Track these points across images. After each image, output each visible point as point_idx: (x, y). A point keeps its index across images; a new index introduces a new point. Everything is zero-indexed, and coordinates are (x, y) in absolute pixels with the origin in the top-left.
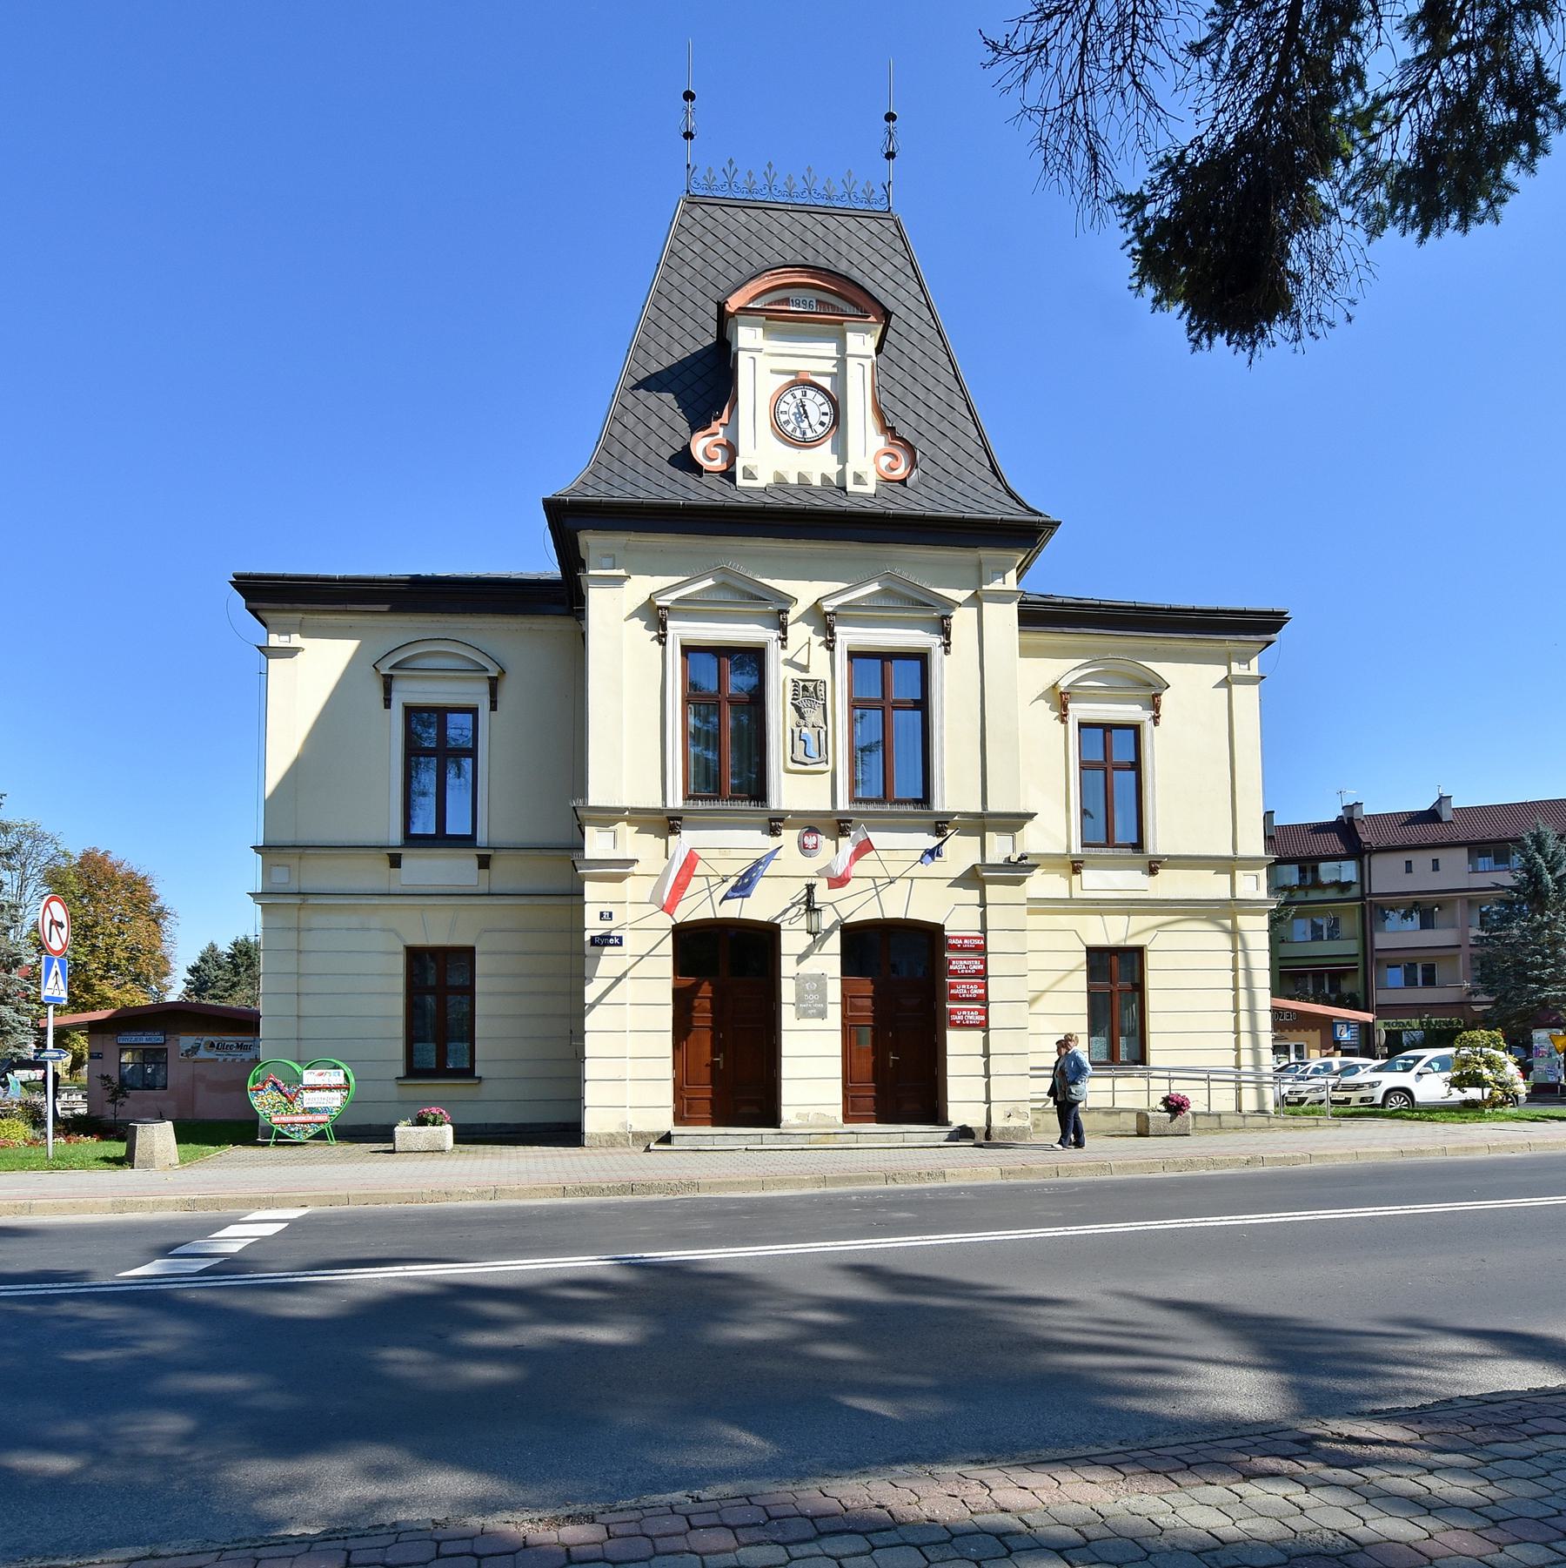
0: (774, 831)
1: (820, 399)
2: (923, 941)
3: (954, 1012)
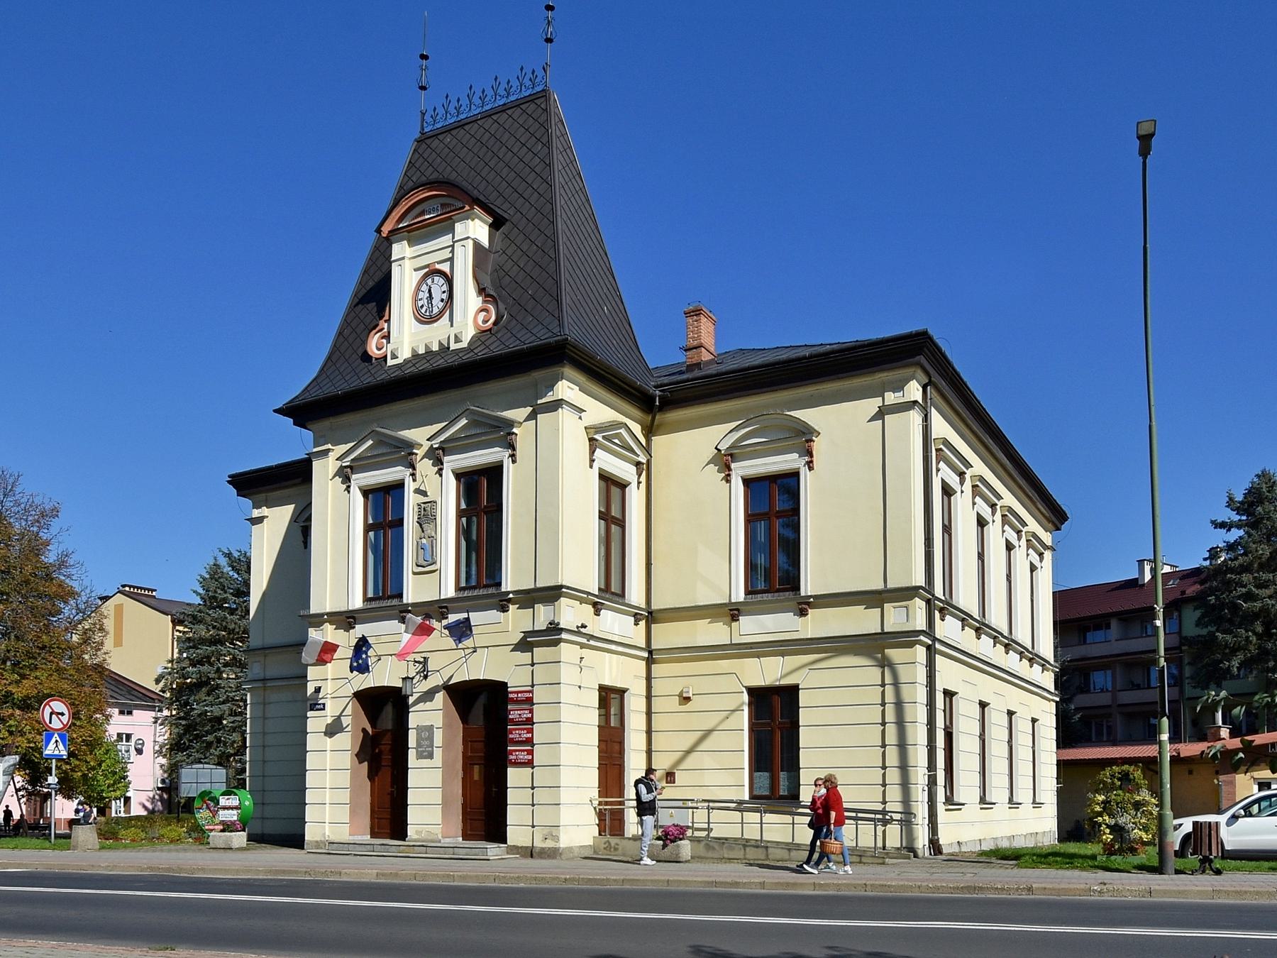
0: (504, 609)
1: (442, 281)
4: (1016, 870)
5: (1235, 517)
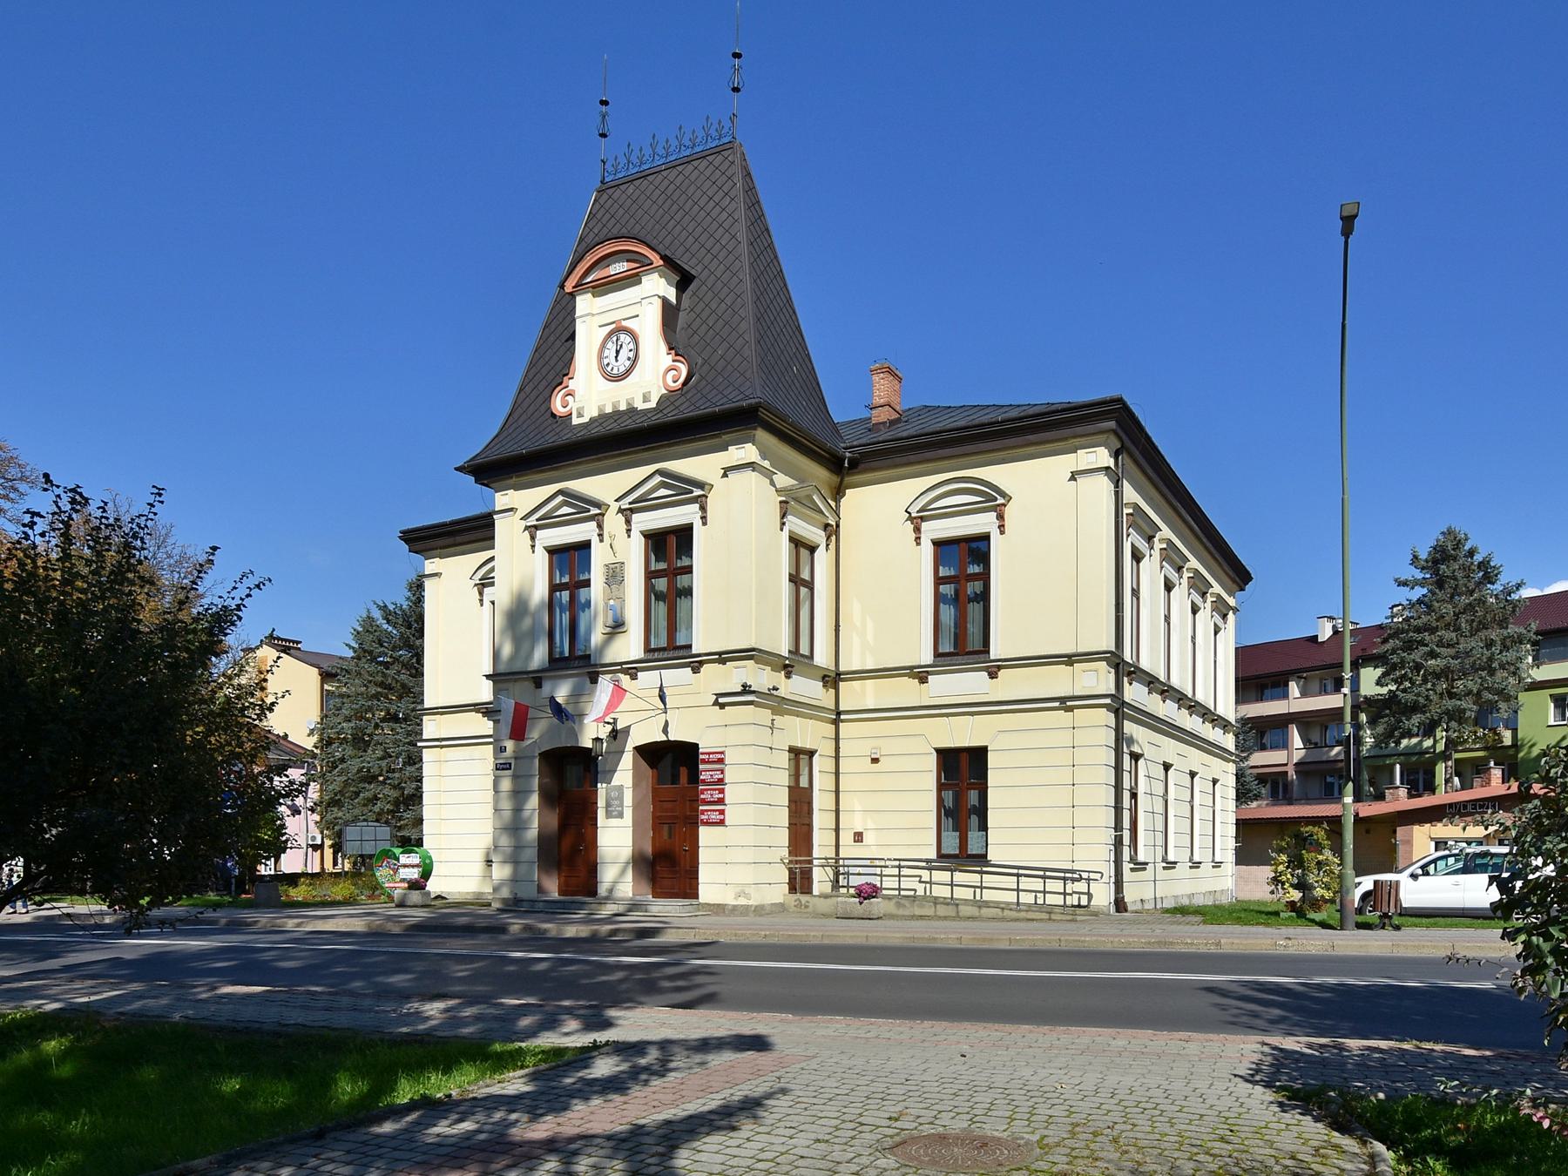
3: (703, 812)
4: (1202, 927)
5: (1419, 575)
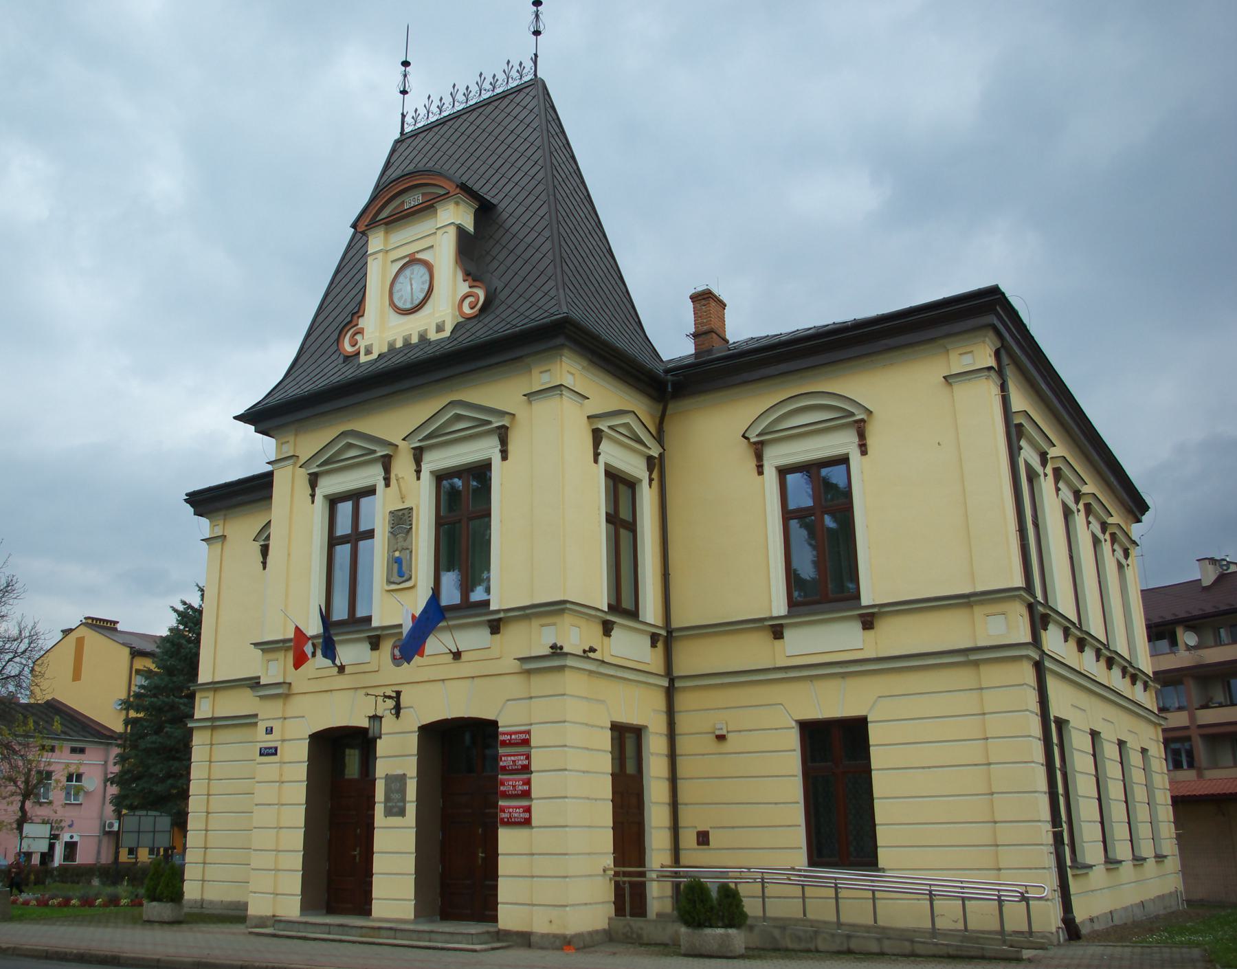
2: (481, 733)
